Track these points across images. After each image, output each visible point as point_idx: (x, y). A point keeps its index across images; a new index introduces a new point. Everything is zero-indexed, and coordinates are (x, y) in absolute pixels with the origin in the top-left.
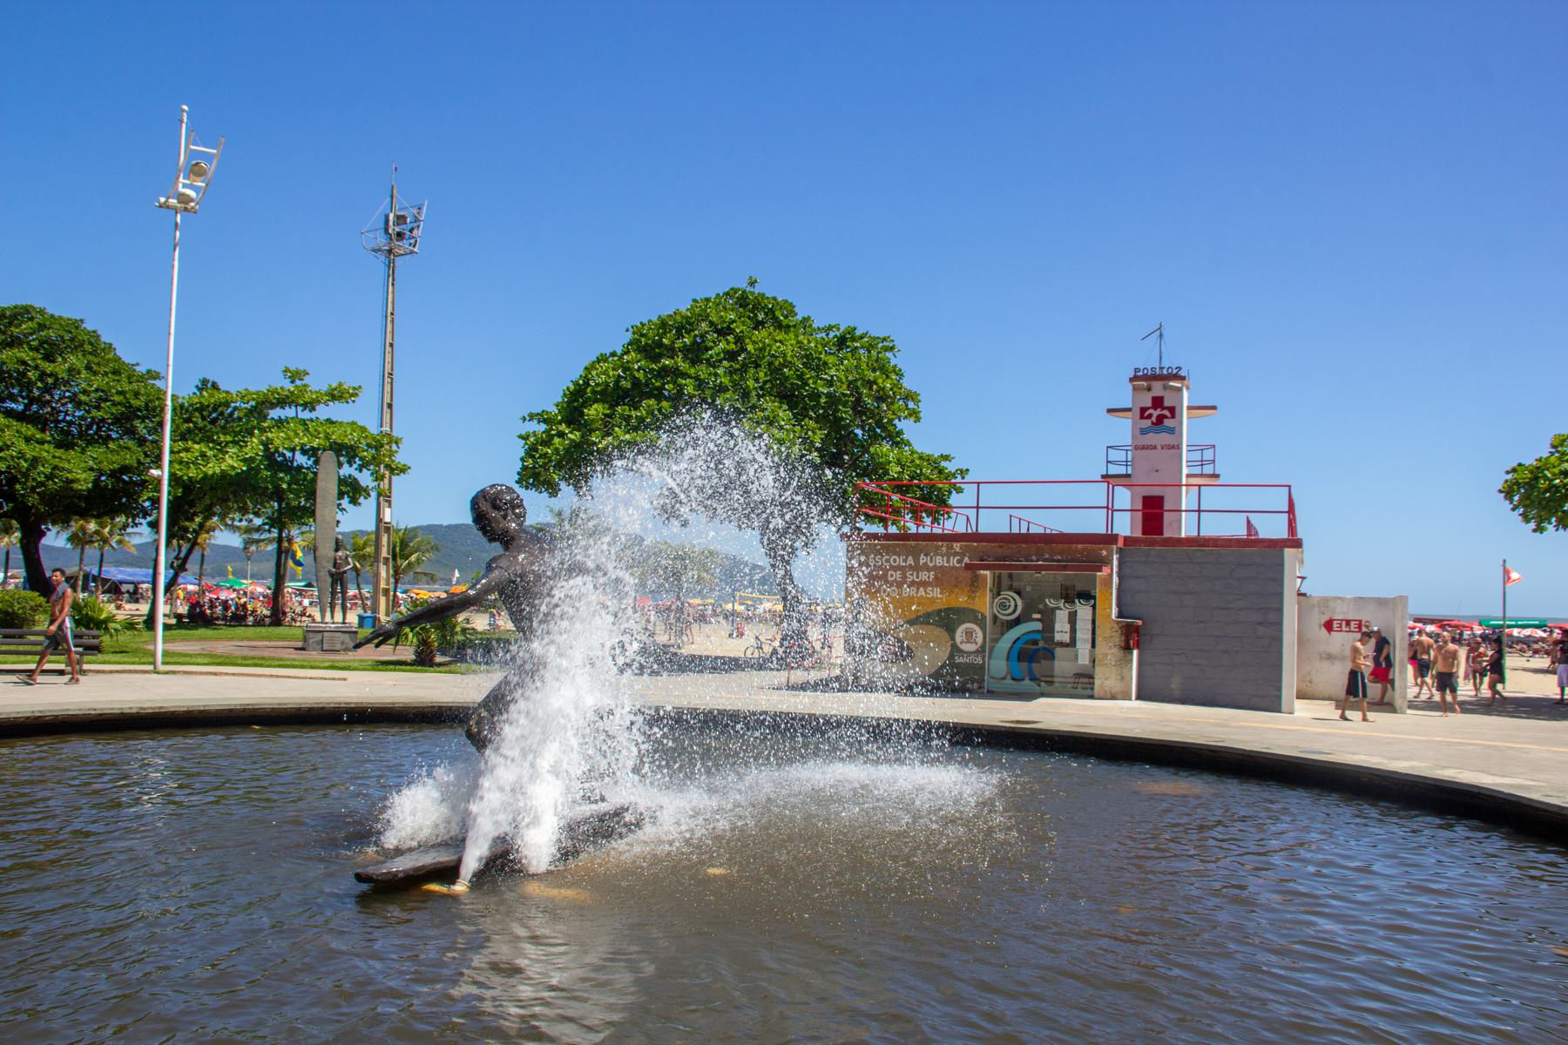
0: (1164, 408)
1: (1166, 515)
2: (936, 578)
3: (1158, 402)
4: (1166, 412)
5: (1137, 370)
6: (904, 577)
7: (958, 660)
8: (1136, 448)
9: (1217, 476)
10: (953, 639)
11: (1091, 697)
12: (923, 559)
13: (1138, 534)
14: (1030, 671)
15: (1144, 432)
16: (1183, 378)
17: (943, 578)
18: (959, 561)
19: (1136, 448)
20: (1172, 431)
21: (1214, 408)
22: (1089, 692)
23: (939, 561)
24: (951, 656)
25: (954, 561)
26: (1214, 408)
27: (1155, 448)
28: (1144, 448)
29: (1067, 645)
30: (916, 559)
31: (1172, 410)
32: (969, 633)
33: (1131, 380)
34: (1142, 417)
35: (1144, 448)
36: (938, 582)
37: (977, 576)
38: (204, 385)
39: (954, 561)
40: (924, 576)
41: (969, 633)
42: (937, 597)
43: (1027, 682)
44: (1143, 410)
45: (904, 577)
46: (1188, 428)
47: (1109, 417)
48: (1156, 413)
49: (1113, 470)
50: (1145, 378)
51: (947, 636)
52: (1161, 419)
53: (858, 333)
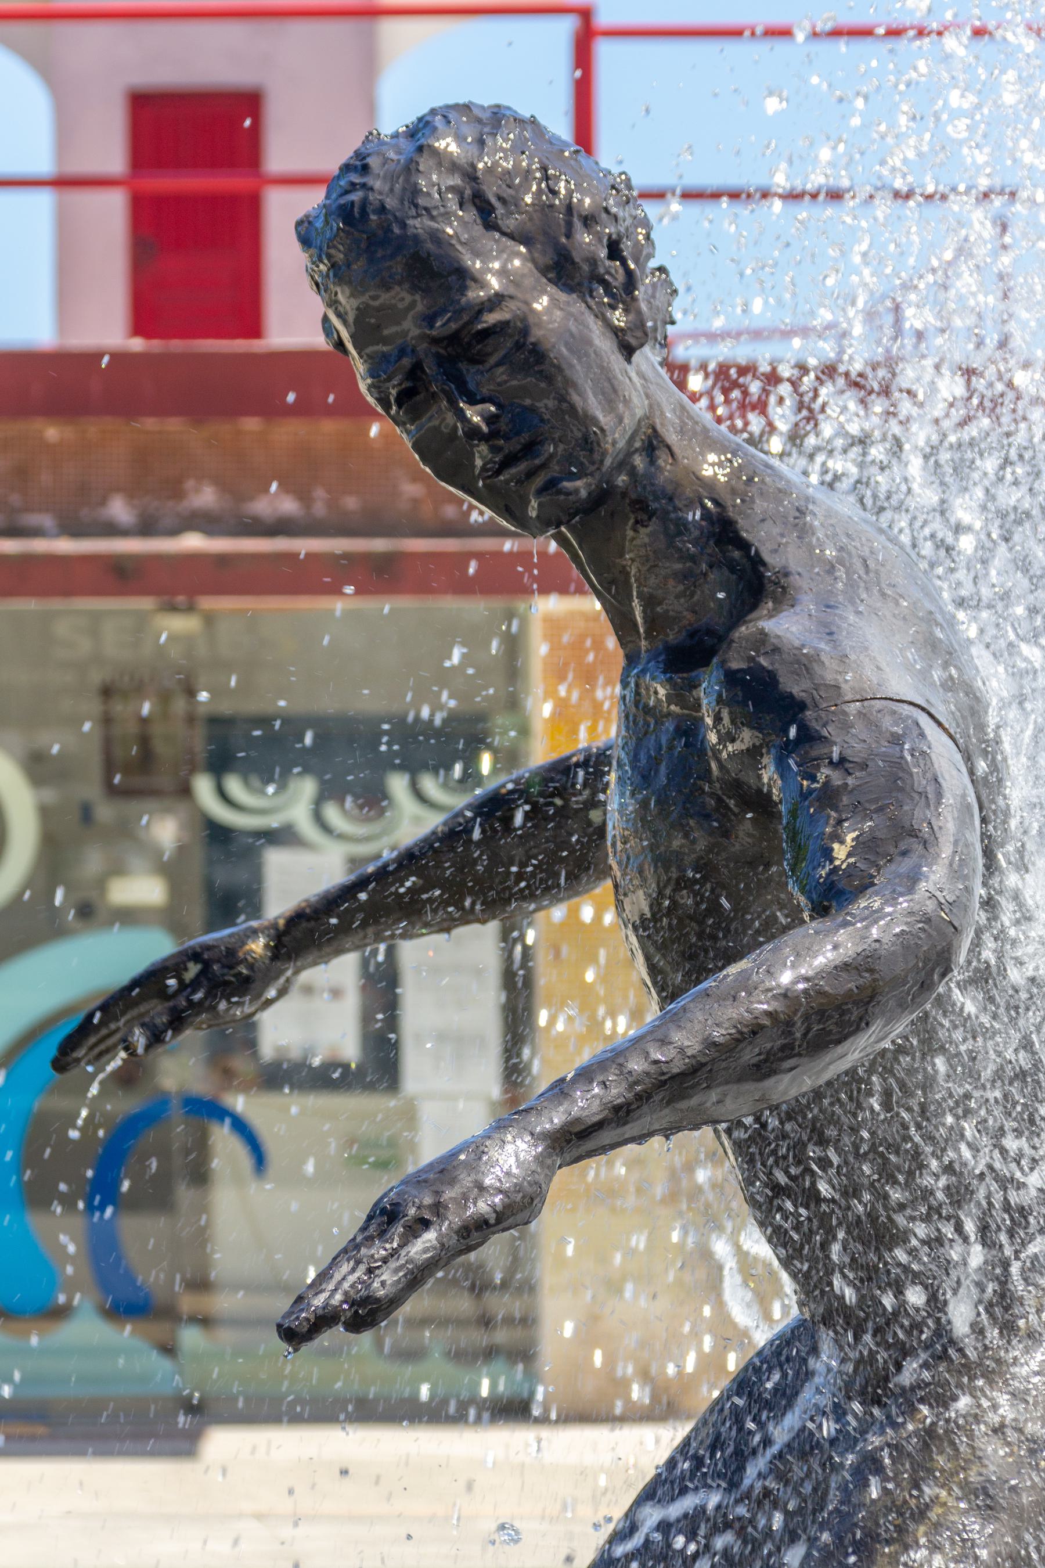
13: (107, 327)
43: (87, 1328)
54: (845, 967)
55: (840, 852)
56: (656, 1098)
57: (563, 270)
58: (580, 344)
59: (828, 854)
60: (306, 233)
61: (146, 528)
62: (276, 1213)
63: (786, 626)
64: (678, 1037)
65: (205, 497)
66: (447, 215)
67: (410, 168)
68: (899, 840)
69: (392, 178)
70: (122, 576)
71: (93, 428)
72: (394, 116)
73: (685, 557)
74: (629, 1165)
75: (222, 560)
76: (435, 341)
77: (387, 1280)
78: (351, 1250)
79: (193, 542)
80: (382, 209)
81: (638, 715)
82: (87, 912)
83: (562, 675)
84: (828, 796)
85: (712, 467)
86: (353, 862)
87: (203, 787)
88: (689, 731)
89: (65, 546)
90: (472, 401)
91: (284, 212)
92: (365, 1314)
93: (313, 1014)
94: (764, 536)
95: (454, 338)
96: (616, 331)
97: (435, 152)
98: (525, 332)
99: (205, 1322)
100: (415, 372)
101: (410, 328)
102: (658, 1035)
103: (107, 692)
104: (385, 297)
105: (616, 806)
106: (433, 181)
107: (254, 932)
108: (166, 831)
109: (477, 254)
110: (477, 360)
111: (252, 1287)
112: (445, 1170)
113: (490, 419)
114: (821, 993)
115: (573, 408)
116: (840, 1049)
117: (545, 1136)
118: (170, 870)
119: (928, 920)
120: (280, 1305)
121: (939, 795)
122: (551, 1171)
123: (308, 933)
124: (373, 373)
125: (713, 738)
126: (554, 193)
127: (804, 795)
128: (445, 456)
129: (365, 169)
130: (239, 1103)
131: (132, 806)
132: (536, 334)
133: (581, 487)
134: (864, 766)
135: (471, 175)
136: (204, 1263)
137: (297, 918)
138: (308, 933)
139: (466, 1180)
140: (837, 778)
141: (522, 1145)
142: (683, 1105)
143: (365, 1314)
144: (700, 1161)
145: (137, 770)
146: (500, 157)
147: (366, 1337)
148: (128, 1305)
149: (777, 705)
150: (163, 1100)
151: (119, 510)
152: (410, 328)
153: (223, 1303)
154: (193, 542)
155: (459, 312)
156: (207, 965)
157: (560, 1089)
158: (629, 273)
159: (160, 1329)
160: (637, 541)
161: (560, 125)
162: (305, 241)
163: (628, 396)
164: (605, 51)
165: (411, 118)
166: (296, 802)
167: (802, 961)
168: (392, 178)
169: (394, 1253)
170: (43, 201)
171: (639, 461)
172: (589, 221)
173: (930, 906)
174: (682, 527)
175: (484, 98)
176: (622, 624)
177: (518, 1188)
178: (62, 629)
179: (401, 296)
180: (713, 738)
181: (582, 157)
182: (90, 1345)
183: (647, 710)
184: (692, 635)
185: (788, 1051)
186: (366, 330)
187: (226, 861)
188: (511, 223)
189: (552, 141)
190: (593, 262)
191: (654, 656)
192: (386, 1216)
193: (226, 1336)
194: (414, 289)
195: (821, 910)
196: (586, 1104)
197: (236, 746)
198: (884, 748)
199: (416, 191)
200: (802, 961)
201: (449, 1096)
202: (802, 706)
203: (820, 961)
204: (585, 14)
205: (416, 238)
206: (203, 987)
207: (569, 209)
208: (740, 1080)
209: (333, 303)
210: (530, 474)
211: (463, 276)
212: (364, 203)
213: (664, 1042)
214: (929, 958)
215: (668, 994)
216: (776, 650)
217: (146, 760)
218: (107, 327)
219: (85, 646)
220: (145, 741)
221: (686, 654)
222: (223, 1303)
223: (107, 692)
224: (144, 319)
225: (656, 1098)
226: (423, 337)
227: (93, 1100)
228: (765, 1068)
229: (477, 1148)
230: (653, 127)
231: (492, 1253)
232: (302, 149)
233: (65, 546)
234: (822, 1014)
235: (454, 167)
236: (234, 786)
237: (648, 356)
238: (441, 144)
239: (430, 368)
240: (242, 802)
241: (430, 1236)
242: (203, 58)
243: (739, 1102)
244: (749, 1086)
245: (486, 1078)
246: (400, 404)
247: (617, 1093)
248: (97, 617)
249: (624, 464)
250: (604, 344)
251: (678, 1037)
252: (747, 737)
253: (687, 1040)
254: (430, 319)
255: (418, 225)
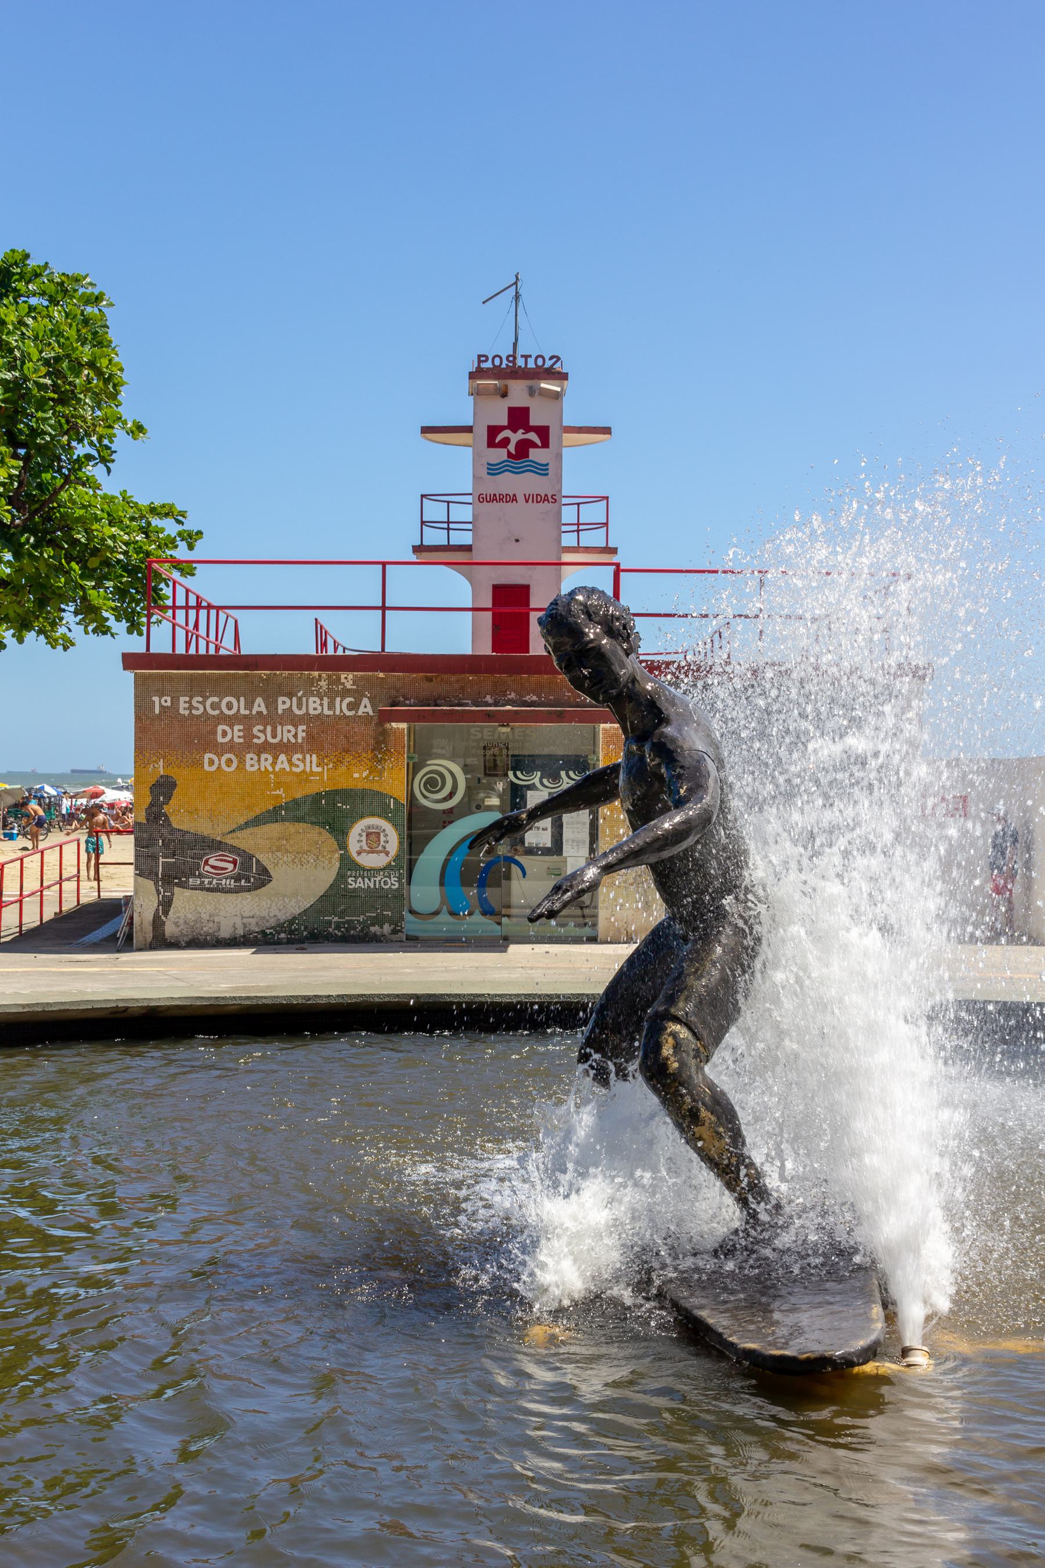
0: (528, 429)
2: (310, 737)
3: (519, 417)
4: (533, 436)
5: (482, 358)
6: (248, 735)
7: (355, 883)
8: (482, 499)
10: (343, 846)
11: (593, 940)
12: (283, 704)
13: (486, 649)
15: (494, 470)
16: (564, 377)
17: (322, 737)
18: (352, 707)
19: (482, 499)
20: (542, 470)
21: (607, 431)
22: (587, 931)
23: (315, 706)
24: (341, 877)
25: (342, 706)
26: (607, 431)
27: (514, 499)
28: (494, 499)
29: (546, 852)
30: (271, 704)
31: (543, 432)
32: (373, 836)
33: (472, 376)
34: (491, 444)
35: (494, 499)
36: (313, 743)
37: (385, 733)
39: (342, 706)
40: (286, 733)
41: (373, 836)
42: (312, 772)
43: (478, 918)
44: (493, 431)
45: (248, 735)
46: (578, 467)
48: (516, 437)
50: (497, 373)
51: (331, 842)
52: (523, 449)
53: (32, 263)
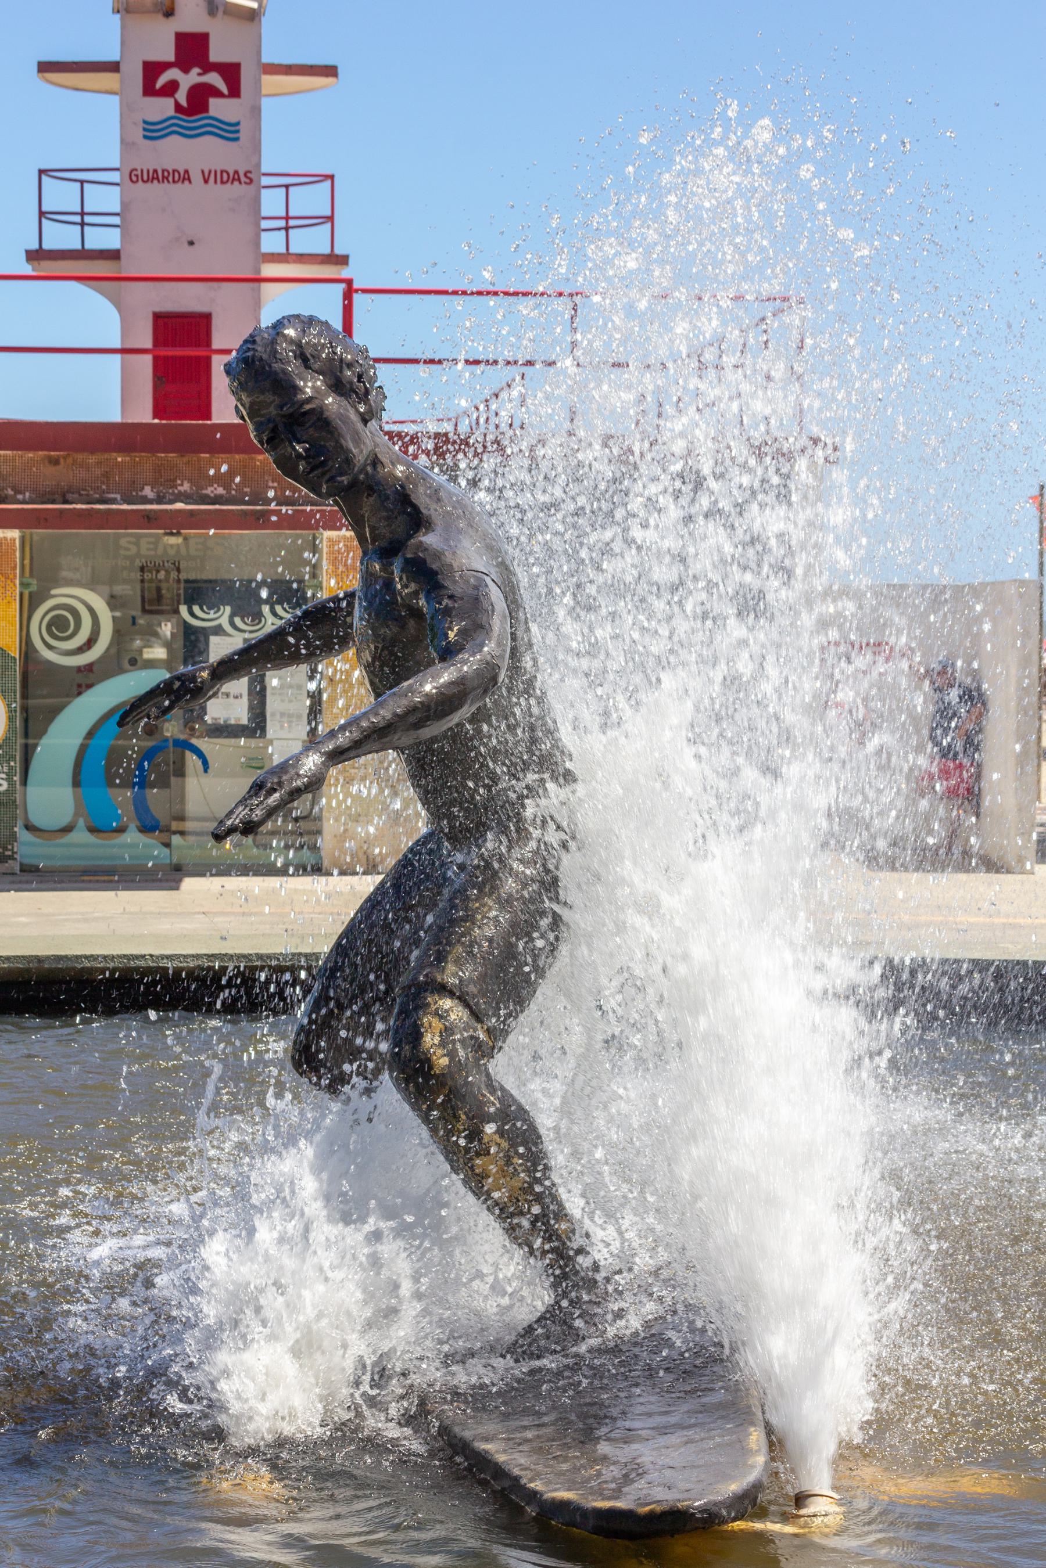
0: (208, 67)
1: (149, 345)
3: (192, 49)
4: (214, 79)
8: (135, 177)
9: (342, 260)
13: (144, 414)
14: (141, 807)
15: (153, 131)
19: (135, 177)
20: (229, 132)
21: (330, 71)
26: (330, 71)
27: (186, 177)
28: (155, 177)
31: (231, 73)
34: (149, 90)
35: (155, 177)
38: (177, 889)
43: (132, 836)
44: (152, 70)
46: (287, 127)
47: (52, 94)
48: (193, 77)
49: (61, 237)
52: (200, 98)
54: (452, 683)
55: (451, 635)
56: (372, 738)
57: (338, 386)
58: (345, 419)
59: (446, 636)
60: (228, 370)
61: (159, 500)
62: (212, 788)
63: (430, 539)
64: (382, 712)
65: (186, 487)
66: (289, 363)
67: (273, 342)
68: (476, 631)
69: (266, 346)
70: (149, 520)
71: (137, 457)
72: (267, 319)
73: (387, 510)
74: (236, 846)
75: (192, 513)
76: (284, 416)
77: (258, 814)
78: (243, 801)
79: (179, 506)
80: (261, 359)
81: (368, 577)
82: (133, 662)
83: (335, 561)
84: (447, 612)
85: (400, 470)
86: (245, 640)
87: (183, 609)
88: (388, 584)
89: (125, 507)
90: (299, 443)
91: (218, 364)
92: (249, 828)
93: (229, 704)
94: (421, 498)
95: (291, 415)
96: (361, 414)
97: (285, 336)
98: (322, 413)
99: (182, 833)
100: (274, 430)
101: (272, 411)
102: (374, 711)
103: (142, 569)
104: (262, 397)
105: (358, 619)
106: (285, 349)
107: (203, 669)
108: (167, 629)
109: (301, 379)
110: (301, 425)
111: (204, 819)
112: (283, 767)
113: (306, 450)
114: (442, 693)
115: (342, 446)
116: (449, 718)
117: (325, 753)
118: (168, 645)
119: (487, 663)
120: (212, 826)
121: (493, 611)
122: (328, 768)
123: (227, 669)
124: (256, 430)
125: (399, 586)
126: (335, 353)
127: (437, 611)
128: (287, 466)
129: (254, 342)
130: (194, 741)
131: (155, 618)
132: (326, 414)
133: (345, 480)
134: (462, 599)
135: (299, 345)
136: (183, 810)
137: (222, 663)
138: (227, 669)
139: (292, 772)
140: (450, 603)
141: (316, 757)
142: (384, 740)
143: (249, 828)
144: (392, 762)
145: (154, 603)
146: (312, 337)
147: (250, 838)
148: (148, 827)
149: (428, 574)
150: (166, 740)
151: (148, 492)
152: (272, 411)
153: (189, 826)
154: (179, 506)
155: (294, 404)
156: (183, 683)
157: (332, 734)
158: (366, 389)
159: (164, 837)
160: (368, 504)
161: (337, 324)
162: (228, 373)
163: (365, 442)
164: (357, 298)
165: (274, 320)
166: (223, 616)
167: (429, 685)
168: (266, 346)
169: (261, 802)
170: (118, 357)
171: (369, 469)
172: (350, 366)
173: (489, 658)
174: (387, 498)
175: (306, 312)
176: (361, 538)
177: (314, 775)
178: (123, 542)
179: (269, 397)
180: (399, 586)
181: (347, 339)
182: (134, 842)
183: (371, 574)
184: (391, 543)
185: (428, 718)
186: (254, 411)
187: (193, 641)
188: (316, 366)
189: (335, 331)
190: (351, 383)
191: (375, 552)
192: (258, 787)
193: (191, 839)
194: (274, 394)
195: (443, 659)
196: (342, 740)
197: (197, 593)
198: (470, 591)
199: (276, 352)
200: (429, 685)
201: (284, 739)
202: (436, 573)
203: (442, 681)
204: (349, 282)
205: (276, 373)
206: (183, 692)
207: (341, 360)
208: (408, 730)
209: (239, 400)
210: (323, 474)
211: (296, 389)
212: (254, 356)
213: (376, 714)
214: (487, 679)
215: (378, 695)
216: (426, 549)
217: (159, 598)
218: (144, 414)
219: (134, 550)
220: (159, 589)
221: (388, 551)
222: (189, 826)
223: (142, 569)
224: (159, 411)
225: (372, 738)
226: (278, 415)
227: (136, 744)
228: (418, 725)
229: (297, 758)
230: (377, 330)
231: (299, 807)
232: (227, 338)
233: (125, 507)
234: (443, 703)
235: (291, 341)
236: (196, 609)
237: (373, 424)
238: (286, 332)
239: (281, 428)
240: (200, 617)
241: (277, 795)
242: (186, 299)
243: (407, 739)
244: (412, 732)
245: (302, 730)
246: (268, 442)
247: (356, 735)
248: (139, 537)
249: (363, 470)
250: (353, 416)
251: (382, 712)
252: (413, 586)
253: (386, 713)
254: (281, 407)
255: (276, 366)
